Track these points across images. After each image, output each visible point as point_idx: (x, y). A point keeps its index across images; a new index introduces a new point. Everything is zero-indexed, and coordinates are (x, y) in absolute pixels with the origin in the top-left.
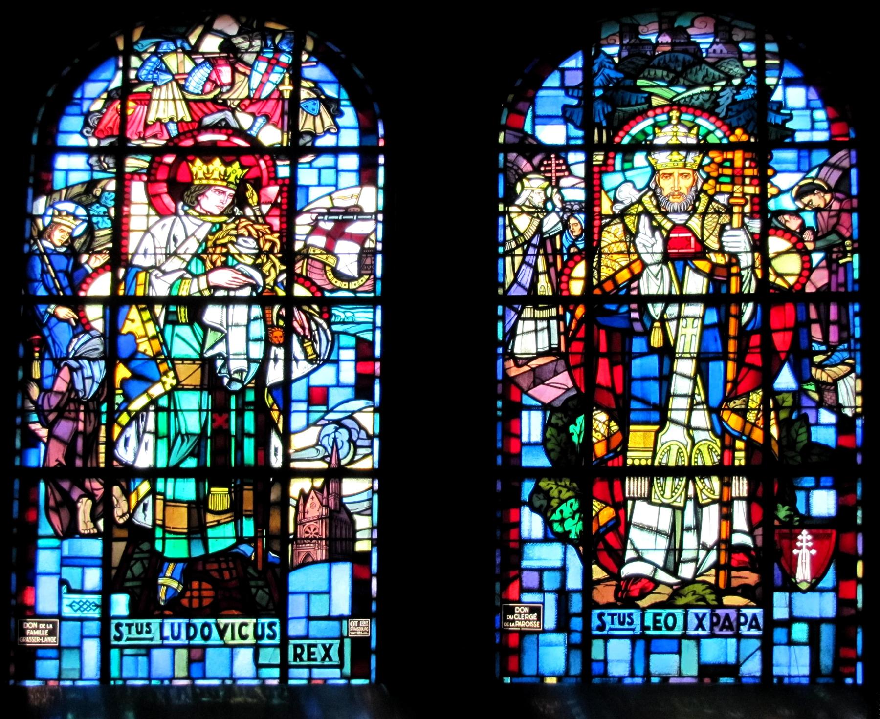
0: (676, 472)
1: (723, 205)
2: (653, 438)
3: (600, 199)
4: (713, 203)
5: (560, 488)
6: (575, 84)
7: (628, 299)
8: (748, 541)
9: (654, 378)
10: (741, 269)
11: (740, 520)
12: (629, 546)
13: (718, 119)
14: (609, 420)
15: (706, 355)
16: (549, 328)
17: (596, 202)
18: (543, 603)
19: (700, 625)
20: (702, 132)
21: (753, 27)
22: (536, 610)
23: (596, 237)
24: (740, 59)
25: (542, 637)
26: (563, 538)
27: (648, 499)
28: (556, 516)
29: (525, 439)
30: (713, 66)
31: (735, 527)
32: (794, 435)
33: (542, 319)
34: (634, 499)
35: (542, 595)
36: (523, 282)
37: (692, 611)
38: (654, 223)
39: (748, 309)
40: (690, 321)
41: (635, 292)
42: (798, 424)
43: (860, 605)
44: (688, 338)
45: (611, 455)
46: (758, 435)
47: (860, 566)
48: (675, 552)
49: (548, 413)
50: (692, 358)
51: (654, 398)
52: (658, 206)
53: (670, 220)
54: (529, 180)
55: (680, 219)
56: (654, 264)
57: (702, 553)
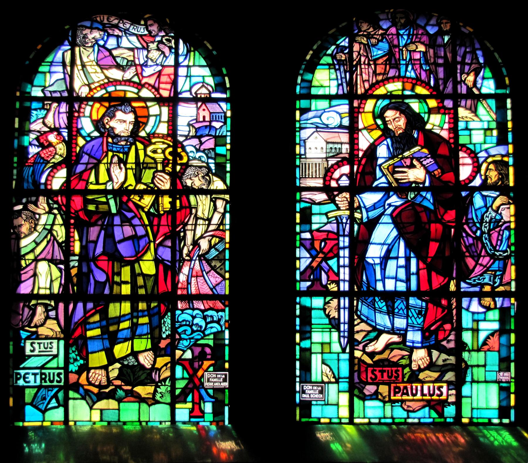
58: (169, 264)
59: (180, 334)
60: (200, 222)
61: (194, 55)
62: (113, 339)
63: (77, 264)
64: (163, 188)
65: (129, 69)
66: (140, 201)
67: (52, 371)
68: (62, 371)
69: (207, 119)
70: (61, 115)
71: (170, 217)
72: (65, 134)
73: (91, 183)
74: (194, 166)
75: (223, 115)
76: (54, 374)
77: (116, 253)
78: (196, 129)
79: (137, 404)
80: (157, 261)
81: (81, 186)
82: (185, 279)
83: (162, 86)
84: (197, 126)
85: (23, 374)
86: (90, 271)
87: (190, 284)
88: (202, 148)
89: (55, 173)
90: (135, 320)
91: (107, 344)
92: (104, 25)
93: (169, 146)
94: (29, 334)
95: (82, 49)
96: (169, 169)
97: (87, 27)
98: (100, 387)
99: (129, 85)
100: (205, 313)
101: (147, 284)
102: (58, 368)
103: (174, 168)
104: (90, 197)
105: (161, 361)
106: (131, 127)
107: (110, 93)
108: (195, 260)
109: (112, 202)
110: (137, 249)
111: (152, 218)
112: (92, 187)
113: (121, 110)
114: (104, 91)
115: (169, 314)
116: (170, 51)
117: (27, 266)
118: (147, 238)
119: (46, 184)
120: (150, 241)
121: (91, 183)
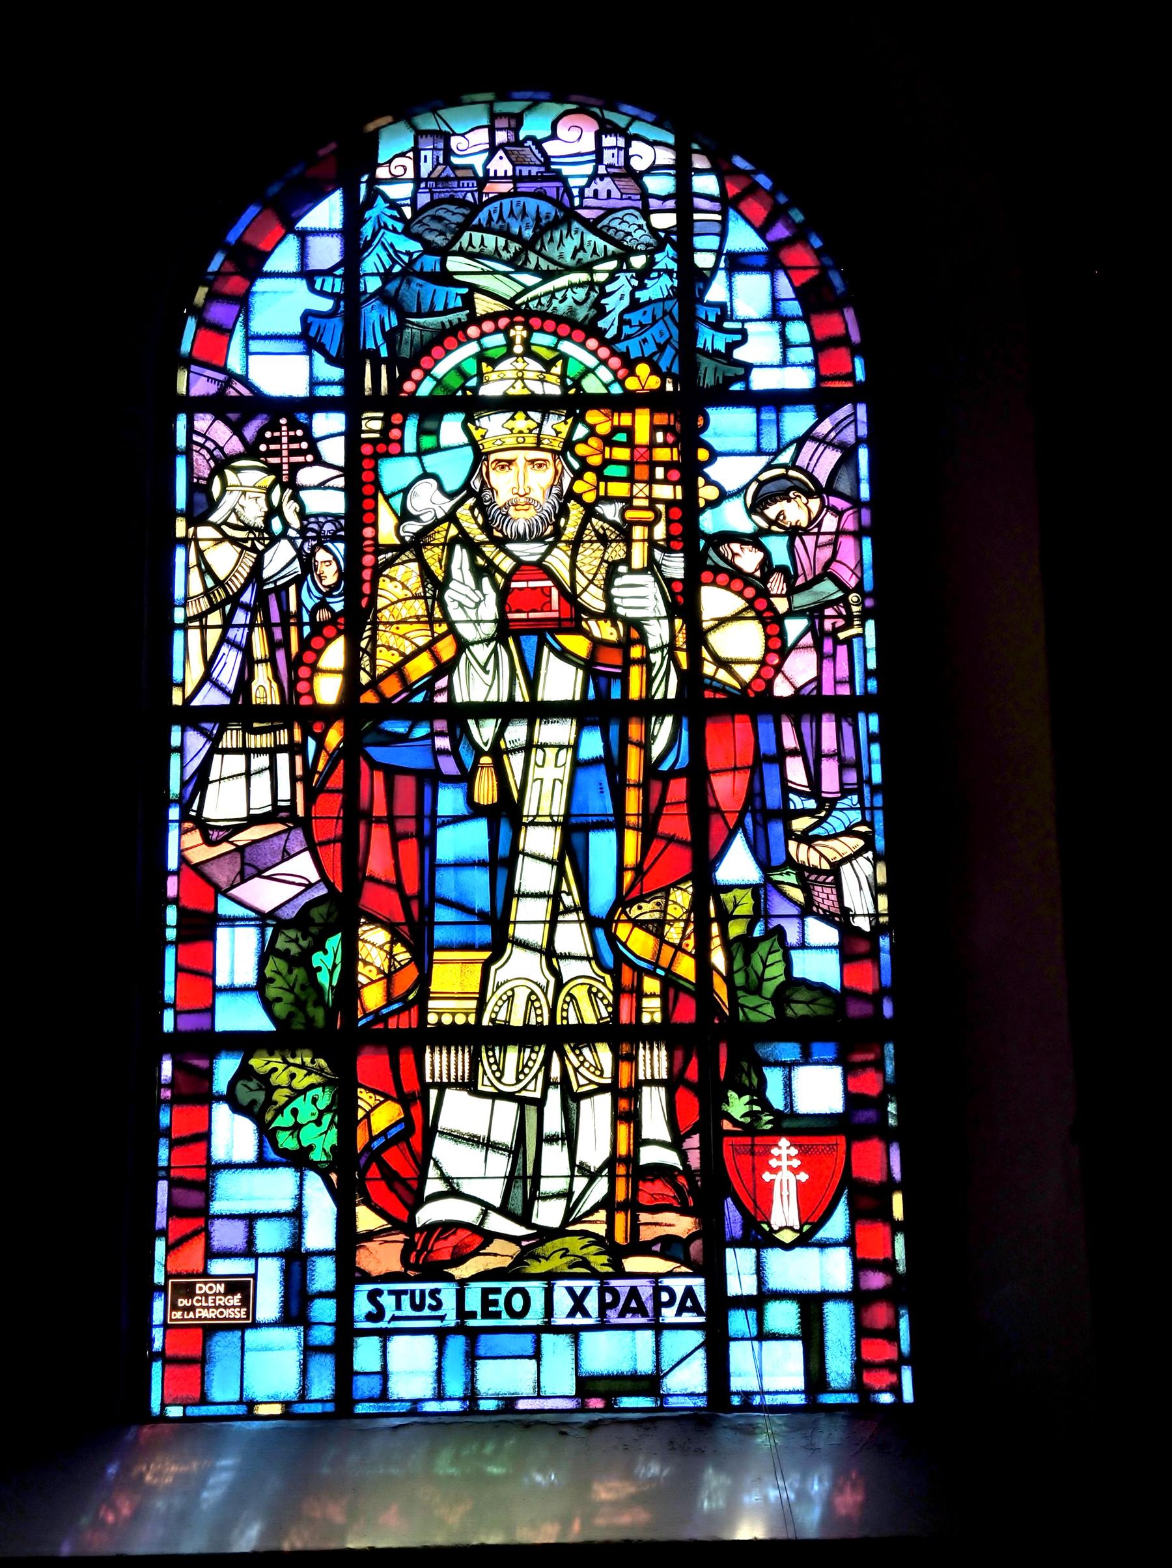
0: (526, 1036)
1: (612, 524)
2: (479, 974)
3: (375, 511)
4: (594, 521)
5: (292, 1069)
6: (327, 266)
7: (428, 712)
8: (671, 1158)
9: (481, 864)
10: (649, 651)
11: (655, 1123)
12: (432, 1172)
13: (604, 342)
14: (392, 943)
15: (583, 819)
16: (273, 768)
17: (367, 518)
18: (254, 1276)
19: (578, 1307)
20: (573, 370)
21: (670, 139)
22: (242, 1288)
23: (366, 588)
24: (646, 212)
25: (250, 1335)
26: (299, 1160)
27: (470, 1086)
28: (286, 1120)
29: (221, 980)
30: (591, 226)
31: (645, 1135)
32: (759, 967)
33: (260, 751)
34: (442, 1087)
35: (253, 1261)
36: (223, 680)
37: (560, 1286)
38: (480, 561)
39: (664, 730)
40: (550, 752)
41: (442, 699)
42: (763, 948)
43: (901, 1268)
44: (546, 789)
45: (396, 1006)
46: (686, 967)
47: (897, 1200)
48: (524, 1185)
49: (269, 931)
50: (554, 824)
51: (482, 901)
52: (486, 528)
53: (509, 554)
54: (237, 470)
55: (529, 551)
56: (481, 642)
57: (580, 1183)
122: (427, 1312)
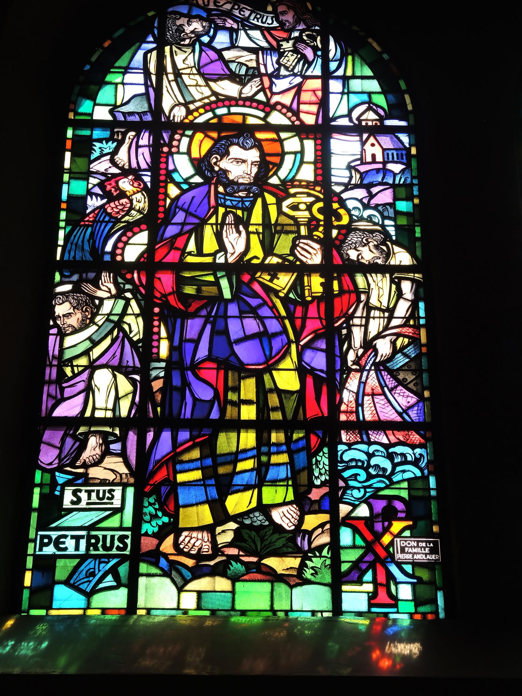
58: (324, 375)
59: (345, 480)
60: (375, 313)
61: (353, 60)
62: (226, 486)
63: (162, 374)
64: (310, 262)
65: (249, 81)
66: (271, 281)
67: (109, 533)
68: (129, 533)
69: (379, 158)
70: (140, 150)
71: (323, 306)
72: (147, 179)
73: (190, 254)
74: (360, 230)
75: (404, 152)
76: (113, 537)
77: (232, 359)
78: (361, 174)
79: (267, 586)
80: (302, 370)
81: (173, 257)
82: (352, 399)
83: (302, 107)
84: (363, 168)
85: (54, 537)
86: (186, 384)
87: (362, 405)
88: (374, 202)
89: (129, 238)
90: (264, 459)
91: (213, 493)
92: (209, 11)
93: (318, 200)
94: (70, 477)
95: (174, 48)
96: (319, 234)
97: (182, 15)
98: (199, 557)
99: (251, 107)
100: (391, 450)
101: (286, 405)
102: (121, 528)
103: (327, 232)
104: (187, 274)
105: (311, 521)
106: (255, 170)
107: (220, 117)
108: (369, 371)
109: (224, 283)
110: (267, 353)
111: (292, 307)
112: (190, 259)
113: (238, 144)
114: (210, 115)
115: (326, 450)
116: (315, 54)
117: (75, 376)
118: (284, 337)
119: (113, 253)
120: (290, 342)
121: (190, 254)
122: (105, 501)
